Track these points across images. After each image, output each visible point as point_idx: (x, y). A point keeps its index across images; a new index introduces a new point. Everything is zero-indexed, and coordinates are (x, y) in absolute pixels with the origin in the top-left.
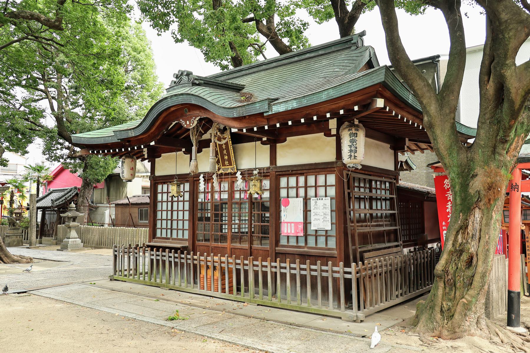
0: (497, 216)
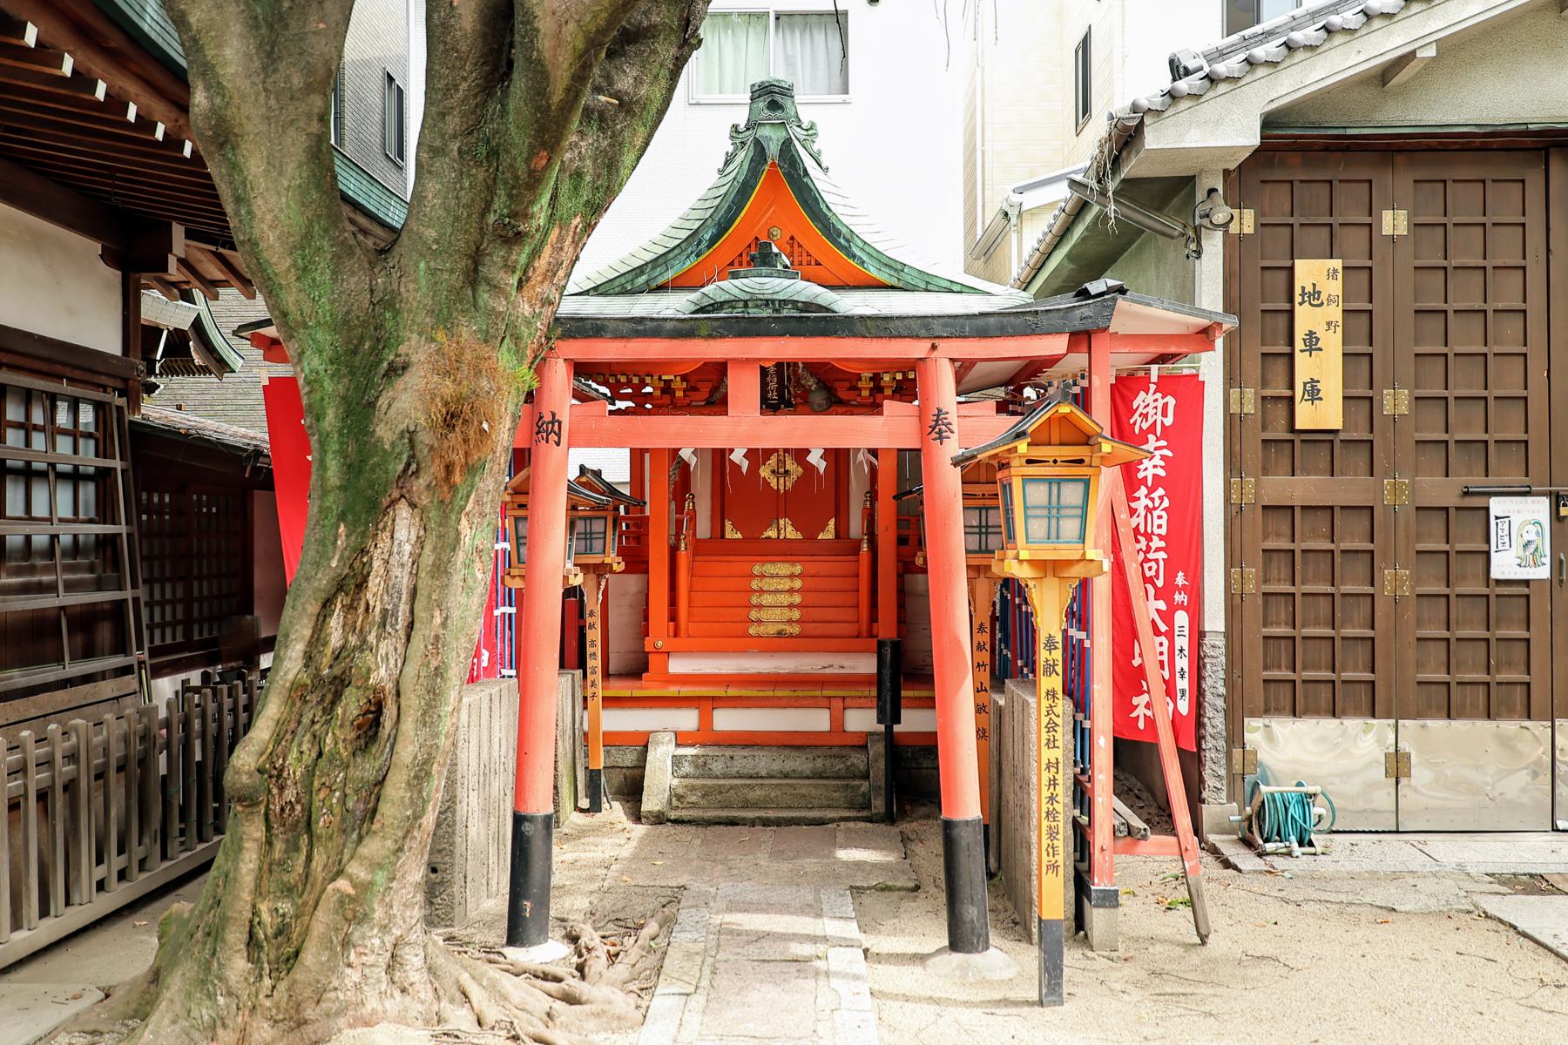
0: (478, 535)
